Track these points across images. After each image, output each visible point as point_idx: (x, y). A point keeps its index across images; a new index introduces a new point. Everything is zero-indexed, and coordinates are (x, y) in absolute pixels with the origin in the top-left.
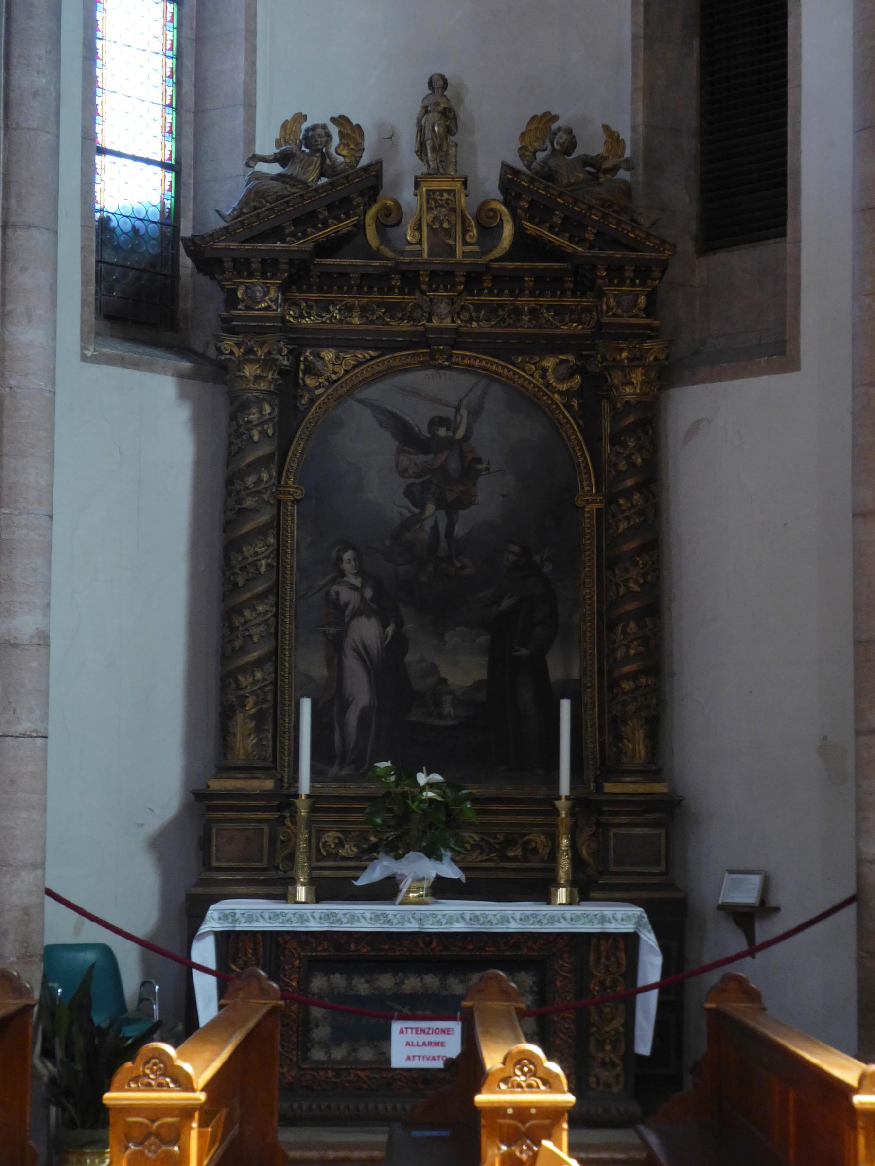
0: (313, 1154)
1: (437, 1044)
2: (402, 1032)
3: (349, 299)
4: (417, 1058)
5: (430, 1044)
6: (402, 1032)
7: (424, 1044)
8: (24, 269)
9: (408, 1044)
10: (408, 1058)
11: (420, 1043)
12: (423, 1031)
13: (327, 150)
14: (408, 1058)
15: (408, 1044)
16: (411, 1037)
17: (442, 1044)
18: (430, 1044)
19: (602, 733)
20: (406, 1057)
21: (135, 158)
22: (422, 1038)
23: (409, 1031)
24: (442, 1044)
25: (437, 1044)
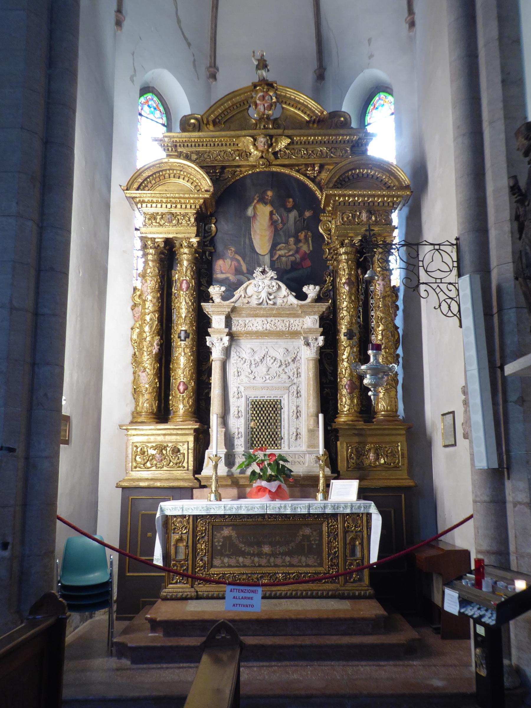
0: (181, 665)
1: (249, 598)
2: (231, 591)
3: (279, 319)
4: (238, 605)
5: (245, 598)
6: (231, 591)
7: (242, 598)
8: (375, 108)
9: (234, 598)
10: (234, 605)
11: (240, 598)
12: (242, 591)
13: (155, 379)
14: (234, 605)
15: (234, 598)
16: (236, 594)
17: (252, 598)
18: (245, 598)
19: (399, 665)
20: (233, 597)
21: (215, 18)
22: (242, 595)
23: (235, 590)
24: (252, 598)
25: (249, 598)
